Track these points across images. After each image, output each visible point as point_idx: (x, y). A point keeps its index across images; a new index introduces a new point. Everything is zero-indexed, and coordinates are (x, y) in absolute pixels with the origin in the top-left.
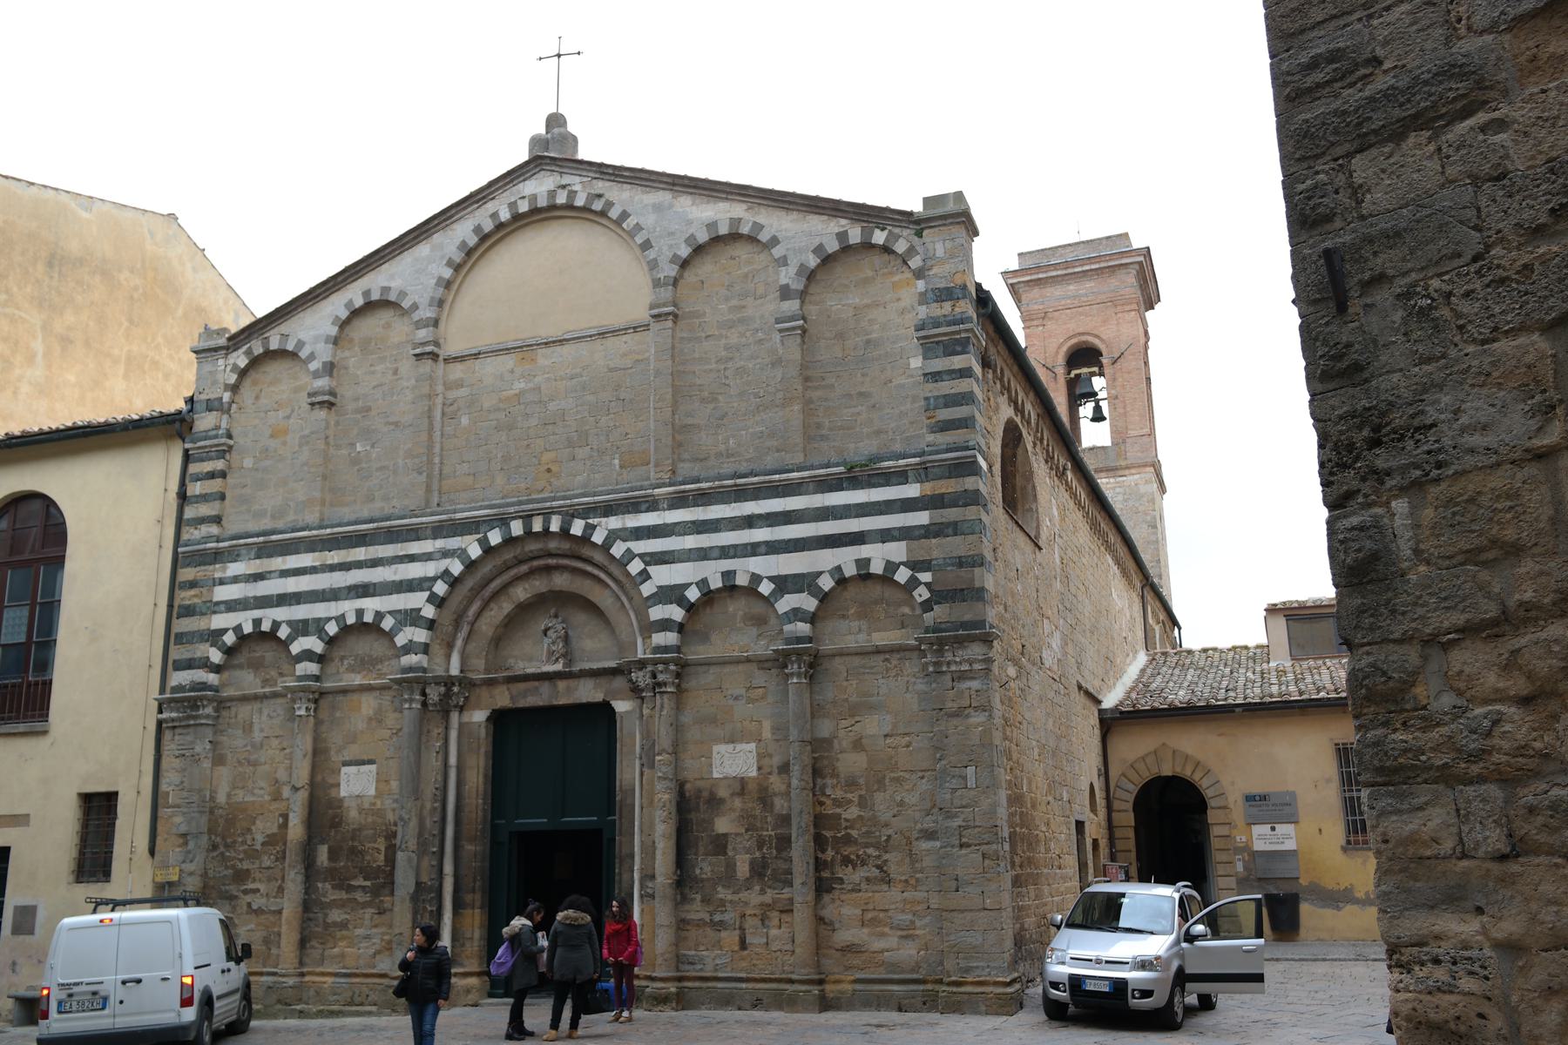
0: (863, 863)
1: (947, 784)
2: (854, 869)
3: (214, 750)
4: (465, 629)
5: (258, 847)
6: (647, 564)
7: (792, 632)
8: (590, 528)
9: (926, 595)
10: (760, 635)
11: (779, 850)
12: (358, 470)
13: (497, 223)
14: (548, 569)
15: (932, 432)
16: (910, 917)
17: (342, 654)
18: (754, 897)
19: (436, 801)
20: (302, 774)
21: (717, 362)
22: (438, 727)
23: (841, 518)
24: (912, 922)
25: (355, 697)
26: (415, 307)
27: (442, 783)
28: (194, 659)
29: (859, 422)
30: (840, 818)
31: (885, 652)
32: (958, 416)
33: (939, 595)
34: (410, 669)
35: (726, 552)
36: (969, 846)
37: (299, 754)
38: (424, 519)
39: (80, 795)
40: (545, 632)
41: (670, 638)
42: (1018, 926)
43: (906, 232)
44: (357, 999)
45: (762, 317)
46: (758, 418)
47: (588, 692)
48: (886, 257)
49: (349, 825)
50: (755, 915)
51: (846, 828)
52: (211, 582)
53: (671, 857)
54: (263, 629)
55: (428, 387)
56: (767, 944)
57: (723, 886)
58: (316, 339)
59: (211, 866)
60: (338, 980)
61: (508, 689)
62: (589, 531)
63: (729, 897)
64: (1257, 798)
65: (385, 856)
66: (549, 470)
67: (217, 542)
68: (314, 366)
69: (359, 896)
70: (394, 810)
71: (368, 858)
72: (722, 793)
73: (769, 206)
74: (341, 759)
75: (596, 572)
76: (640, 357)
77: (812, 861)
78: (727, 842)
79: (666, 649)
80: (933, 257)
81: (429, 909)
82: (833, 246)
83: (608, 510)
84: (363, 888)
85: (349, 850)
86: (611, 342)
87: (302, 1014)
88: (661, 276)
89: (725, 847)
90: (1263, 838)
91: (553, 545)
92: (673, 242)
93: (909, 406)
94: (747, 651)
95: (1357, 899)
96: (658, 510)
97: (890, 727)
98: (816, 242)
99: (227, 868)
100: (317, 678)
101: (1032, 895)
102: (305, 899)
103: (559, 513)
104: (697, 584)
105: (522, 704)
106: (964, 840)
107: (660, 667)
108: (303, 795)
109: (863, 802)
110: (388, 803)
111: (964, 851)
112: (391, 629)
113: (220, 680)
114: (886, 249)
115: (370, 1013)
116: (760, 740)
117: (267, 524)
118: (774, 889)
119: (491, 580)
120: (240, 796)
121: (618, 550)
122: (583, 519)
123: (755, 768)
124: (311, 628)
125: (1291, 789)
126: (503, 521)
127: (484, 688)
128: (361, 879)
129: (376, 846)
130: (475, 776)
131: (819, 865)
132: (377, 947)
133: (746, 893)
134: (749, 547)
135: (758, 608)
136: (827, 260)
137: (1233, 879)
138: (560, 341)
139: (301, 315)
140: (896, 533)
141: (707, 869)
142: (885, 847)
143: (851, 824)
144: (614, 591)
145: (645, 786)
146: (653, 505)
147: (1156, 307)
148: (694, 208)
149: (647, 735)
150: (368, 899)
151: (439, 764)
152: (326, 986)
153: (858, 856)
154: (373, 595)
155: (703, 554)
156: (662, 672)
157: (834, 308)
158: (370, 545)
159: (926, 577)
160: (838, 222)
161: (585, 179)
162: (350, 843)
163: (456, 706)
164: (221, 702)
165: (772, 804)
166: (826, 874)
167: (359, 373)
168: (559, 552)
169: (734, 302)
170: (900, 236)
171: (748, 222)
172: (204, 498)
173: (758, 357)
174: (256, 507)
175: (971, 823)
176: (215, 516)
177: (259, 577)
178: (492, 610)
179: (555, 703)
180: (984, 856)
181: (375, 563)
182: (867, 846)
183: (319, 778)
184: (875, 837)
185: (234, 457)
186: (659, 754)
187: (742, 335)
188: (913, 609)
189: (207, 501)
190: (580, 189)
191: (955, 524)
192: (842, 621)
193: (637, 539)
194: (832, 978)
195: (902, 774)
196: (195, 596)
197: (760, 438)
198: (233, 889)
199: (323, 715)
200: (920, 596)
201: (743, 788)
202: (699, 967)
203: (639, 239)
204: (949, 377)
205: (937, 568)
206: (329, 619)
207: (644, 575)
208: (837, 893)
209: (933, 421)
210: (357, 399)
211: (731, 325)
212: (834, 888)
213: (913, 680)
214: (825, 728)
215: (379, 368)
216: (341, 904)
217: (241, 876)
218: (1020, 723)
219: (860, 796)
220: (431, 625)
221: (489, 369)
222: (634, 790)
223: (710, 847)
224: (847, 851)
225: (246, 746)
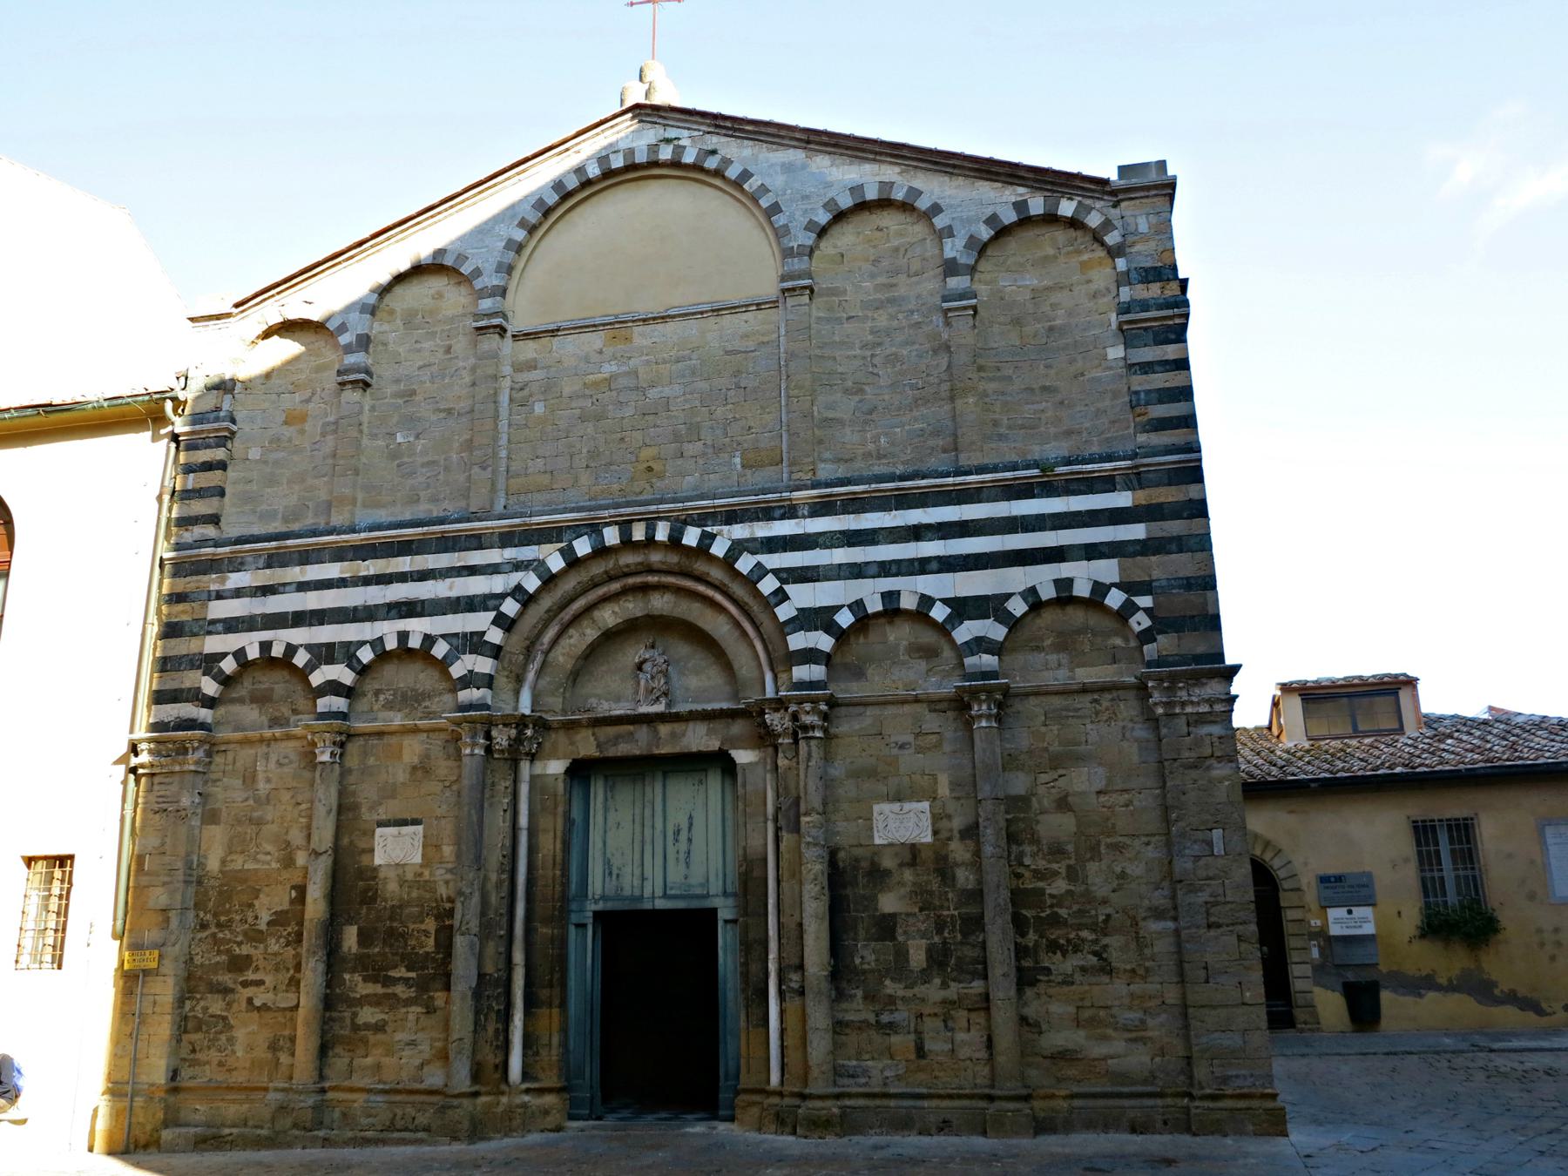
0: (1076, 950)
1: (1187, 851)
2: (1064, 956)
3: (204, 804)
5: (263, 927)
6: (783, 581)
7: (975, 665)
8: (707, 539)
9: (1146, 622)
10: (930, 670)
12: (398, 466)
13: (584, 179)
14: (645, 589)
16: (1139, 1015)
17: (377, 687)
18: (934, 992)
19: (503, 872)
20: (324, 835)
22: (505, 779)
23: (1033, 531)
24: (1143, 1022)
25: (394, 740)
26: (477, 272)
27: (510, 850)
28: (182, 691)
29: (1043, 422)
30: (1044, 894)
31: (1092, 691)
33: (1162, 623)
34: (471, 706)
35: (886, 569)
36: (1219, 926)
37: (320, 810)
38: (489, 524)
40: (640, 667)
41: (816, 672)
43: (1099, 204)
44: (399, 1124)
45: (918, 297)
46: (916, 413)
48: (1072, 233)
49: (385, 900)
50: (936, 1015)
51: (1052, 906)
52: (205, 596)
53: (825, 943)
54: (273, 654)
56: (953, 1050)
57: (893, 979)
59: (198, 950)
60: (373, 1098)
61: (593, 734)
62: (707, 542)
63: (900, 993)
64: (1333, 879)
65: (436, 939)
66: (650, 469)
67: (215, 546)
68: (345, 339)
69: (400, 990)
70: (447, 882)
71: (412, 942)
72: (888, 862)
73: (930, 170)
74: (376, 817)
75: (710, 592)
76: (766, 339)
78: (895, 925)
79: (812, 685)
80: (1136, 233)
81: (496, 1008)
82: (1009, 217)
83: (732, 516)
84: (406, 981)
86: (728, 320)
87: (326, 1142)
90: (1339, 922)
91: (656, 557)
92: (810, 207)
93: (1107, 403)
94: (913, 690)
95: (1441, 985)
96: (796, 517)
97: (1104, 783)
98: (989, 212)
99: (219, 952)
100: (343, 716)
103: (667, 519)
104: (850, 606)
105: (612, 752)
106: (1212, 919)
107: (808, 706)
108: (324, 863)
110: (440, 874)
111: (1213, 933)
112: (444, 657)
113: (214, 718)
114: (1074, 223)
115: (420, 1142)
116: (935, 798)
117: (276, 526)
118: (960, 982)
119: (572, 600)
120: (238, 863)
121: (745, 564)
122: (699, 526)
123: (929, 832)
125: (1367, 869)
126: (594, 529)
127: (561, 733)
128: (403, 969)
129: (423, 927)
130: (551, 841)
131: (1021, 952)
132: (427, 1056)
133: (923, 988)
134: (916, 564)
135: (928, 637)
136: (1002, 232)
137: (1309, 966)
138: (663, 318)
140: (1105, 550)
142: (1104, 928)
143: (1059, 900)
144: (732, 617)
145: (785, 856)
146: (790, 512)
148: (834, 169)
150: (414, 995)
152: (356, 1105)
154: (421, 615)
155: (856, 571)
156: (808, 713)
158: (417, 554)
159: (1145, 601)
160: (1014, 190)
161: (696, 133)
163: (527, 754)
164: (214, 744)
165: (954, 878)
168: (664, 567)
169: (881, 280)
170: (1092, 208)
173: (914, 343)
175: (1221, 899)
176: (212, 515)
178: (571, 637)
179: (656, 752)
180: (1240, 938)
182: (1080, 927)
183: (345, 841)
184: (1091, 917)
185: (237, 445)
186: (806, 814)
188: (1126, 640)
189: (201, 497)
191: (1179, 539)
192: (1035, 654)
194: (1042, 1092)
195: (1120, 839)
196: (184, 612)
197: (919, 436)
199: (353, 761)
200: (1139, 624)
201: (914, 857)
202: (863, 1080)
203: (765, 203)
204: (1161, 369)
205: (1159, 591)
206: (362, 643)
207: (780, 596)
208: (1042, 987)
209: (1145, 418)
210: (398, 381)
211: (879, 306)
212: (1040, 981)
213: (1130, 725)
215: (427, 345)
216: (375, 1001)
217: (238, 964)
220: (496, 652)
221: (569, 348)
222: (765, 860)
223: (874, 930)
224: (1054, 934)
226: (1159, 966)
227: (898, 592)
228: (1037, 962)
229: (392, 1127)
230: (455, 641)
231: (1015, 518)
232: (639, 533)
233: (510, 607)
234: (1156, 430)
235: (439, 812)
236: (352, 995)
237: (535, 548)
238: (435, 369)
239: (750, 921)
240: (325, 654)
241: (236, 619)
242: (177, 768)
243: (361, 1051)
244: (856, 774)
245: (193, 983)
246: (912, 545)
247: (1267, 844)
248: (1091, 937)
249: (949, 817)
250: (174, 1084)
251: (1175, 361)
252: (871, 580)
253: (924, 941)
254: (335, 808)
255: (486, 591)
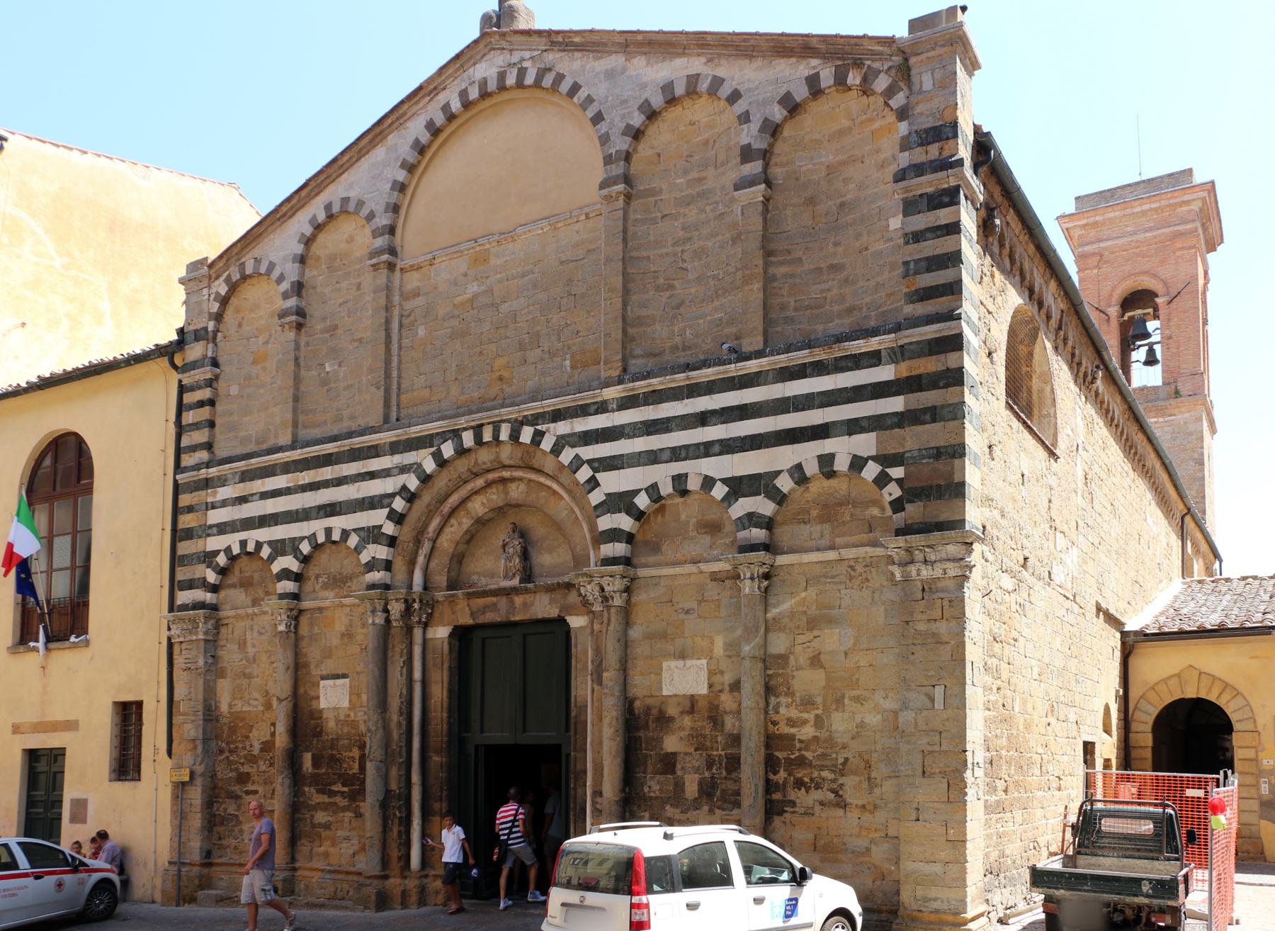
2: (807, 792)
4: (426, 546)
6: (595, 470)
7: (746, 539)
11: (729, 771)
12: (328, 391)
15: (912, 302)
21: (673, 245)
23: (803, 410)
28: (194, 580)
32: (942, 281)
33: (912, 493)
35: (677, 454)
39: (115, 703)
42: (995, 854)
45: (723, 187)
46: (716, 303)
47: (543, 607)
51: (800, 750)
52: (204, 507)
55: (384, 299)
58: (285, 259)
69: (338, 799)
71: (345, 766)
72: (672, 711)
75: (549, 482)
77: (761, 784)
78: (675, 762)
84: (343, 793)
85: (329, 758)
88: (613, 151)
89: (674, 766)
92: (626, 111)
97: (852, 642)
98: (783, 91)
101: (1019, 819)
102: (294, 802)
104: (646, 490)
105: (481, 620)
109: (819, 722)
110: (360, 716)
115: (346, 908)
118: (723, 810)
119: (448, 496)
120: (239, 706)
122: (532, 425)
123: (706, 685)
124: (288, 549)
129: (351, 754)
131: (770, 787)
133: (695, 813)
134: (702, 447)
139: (272, 236)
140: (865, 424)
141: (656, 787)
142: (842, 769)
143: (806, 744)
147: (1219, 248)
149: (598, 651)
151: (403, 680)
153: (812, 780)
154: (340, 514)
155: (652, 458)
157: (804, 168)
159: (897, 472)
160: (808, 64)
161: (536, 53)
162: (330, 751)
166: (777, 796)
167: (326, 291)
169: (694, 175)
170: (880, 72)
171: (707, 76)
172: (196, 426)
173: (718, 235)
174: (243, 434)
175: (936, 748)
177: (243, 500)
178: (452, 526)
181: (339, 482)
182: (822, 768)
183: (302, 691)
184: (832, 759)
187: (703, 211)
188: (883, 509)
189: (198, 429)
190: (526, 57)
193: (586, 444)
197: (717, 326)
198: (236, 789)
200: (890, 494)
201: (693, 707)
206: (303, 538)
210: (324, 319)
211: (689, 200)
212: (785, 811)
214: (779, 644)
216: (325, 807)
217: (243, 778)
218: (1016, 640)
219: (817, 716)
220: (392, 542)
222: (586, 706)
225: (241, 660)
226: (886, 804)
227: (686, 475)
228: (785, 796)
229: (334, 898)
230: (362, 533)
231: (789, 398)
232: (487, 436)
233: (399, 504)
234: (922, 300)
235: (358, 669)
236: (310, 802)
237: (414, 453)
238: (349, 305)
239: (578, 755)
240: (279, 548)
241: (225, 523)
242: (194, 638)
243: (317, 843)
244: (649, 637)
245: (217, 791)
246: (700, 430)
247: (1226, 686)
248: (831, 776)
249: (722, 673)
250: (207, 861)
251: (946, 226)
252: (664, 465)
253: (697, 776)
254: (292, 666)
255: (382, 492)
